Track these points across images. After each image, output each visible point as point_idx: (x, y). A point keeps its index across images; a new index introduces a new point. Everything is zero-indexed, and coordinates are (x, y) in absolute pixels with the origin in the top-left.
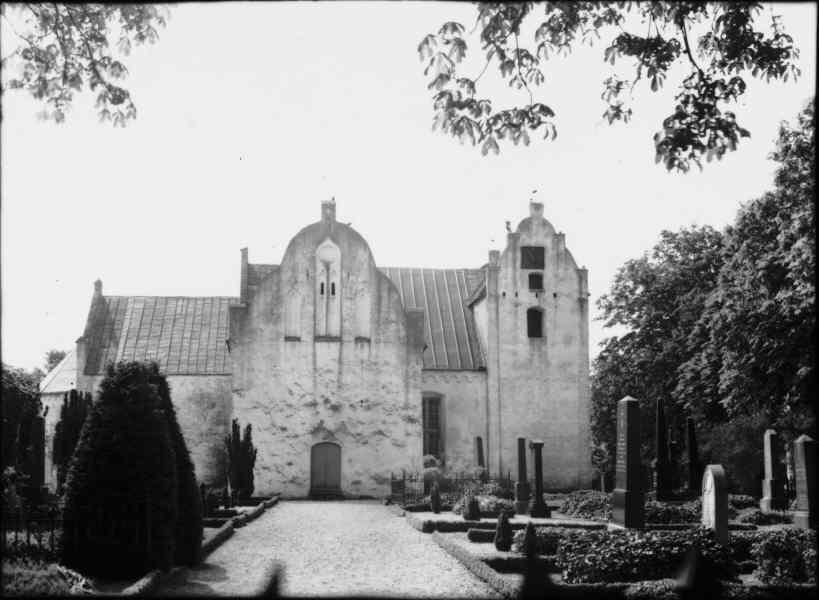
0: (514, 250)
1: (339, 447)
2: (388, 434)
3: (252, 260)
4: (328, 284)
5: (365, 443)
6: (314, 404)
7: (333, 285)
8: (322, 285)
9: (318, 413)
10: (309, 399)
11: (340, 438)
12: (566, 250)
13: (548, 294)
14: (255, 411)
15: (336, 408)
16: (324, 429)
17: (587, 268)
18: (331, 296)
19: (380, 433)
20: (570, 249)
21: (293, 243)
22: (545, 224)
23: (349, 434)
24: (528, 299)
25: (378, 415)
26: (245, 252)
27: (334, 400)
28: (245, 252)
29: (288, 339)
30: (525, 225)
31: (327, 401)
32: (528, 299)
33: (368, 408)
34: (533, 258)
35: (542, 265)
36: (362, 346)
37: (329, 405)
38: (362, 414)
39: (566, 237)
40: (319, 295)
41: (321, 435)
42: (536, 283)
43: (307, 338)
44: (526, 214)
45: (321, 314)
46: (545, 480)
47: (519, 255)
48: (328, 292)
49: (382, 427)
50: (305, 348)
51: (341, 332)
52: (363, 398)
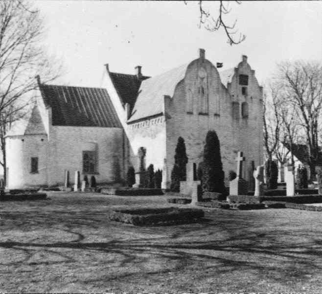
6: (198, 144)
10: (197, 141)
22: (248, 66)
28: (107, 66)
30: (241, 64)
36: (217, 118)
37: (117, 162)
39: (256, 72)
42: (244, 91)
43: (195, 113)
44: (240, 60)
47: (238, 77)
50: (195, 117)
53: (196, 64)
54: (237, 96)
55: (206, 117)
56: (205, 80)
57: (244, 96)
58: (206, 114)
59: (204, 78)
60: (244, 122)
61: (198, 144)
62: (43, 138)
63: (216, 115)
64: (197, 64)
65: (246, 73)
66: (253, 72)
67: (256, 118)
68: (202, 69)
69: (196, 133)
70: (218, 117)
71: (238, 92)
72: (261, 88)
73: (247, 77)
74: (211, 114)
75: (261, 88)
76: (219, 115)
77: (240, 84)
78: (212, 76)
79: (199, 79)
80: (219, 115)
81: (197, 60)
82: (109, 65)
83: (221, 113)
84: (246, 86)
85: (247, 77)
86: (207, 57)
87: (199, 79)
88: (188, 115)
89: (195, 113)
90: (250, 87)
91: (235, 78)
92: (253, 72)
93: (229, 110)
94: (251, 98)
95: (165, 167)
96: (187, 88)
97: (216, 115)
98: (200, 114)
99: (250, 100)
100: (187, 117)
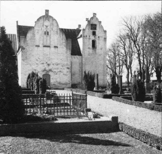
0: (89, 25)
1: (50, 75)
2: (63, 72)
3: (19, 24)
4: (47, 32)
5: (57, 74)
6: (43, 64)
7: (48, 32)
8: (45, 32)
9: (44, 66)
10: (42, 62)
11: (50, 73)
12: (102, 26)
13: (97, 37)
14: (28, 65)
15: (49, 65)
16: (46, 70)
17: (106, 30)
18: (47, 36)
19: (60, 71)
20: (102, 25)
21: (40, 18)
22: (97, 19)
23: (52, 71)
24: (92, 38)
25: (60, 66)
26: (17, 22)
27: (49, 63)
28: (17, 22)
29: (36, 46)
30: (92, 18)
31: (46, 63)
32: (92, 38)
33: (57, 65)
34: (93, 26)
35: (95, 29)
36: (56, 49)
37: (47, 64)
38: (55, 67)
39: (102, 22)
40: (44, 35)
41: (45, 72)
42: (94, 34)
43: (41, 46)
44: (92, 16)
45: (45, 40)
46: (99, 84)
47: (90, 26)
48: (47, 34)
49: (61, 70)
50: (41, 48)
51: (50, 44)
52: (56, 62)
53: (42, 18)
54: (89, 36)
55: (48, 48)
56: (49, 27)
57: (94, 36)
58: (49, 47)
59: (48, 26)
60: (94, 52)
61: (43, 64)
62: (103, 50)
63: (56, 47)
64: (44, 19)
65: (95, 23)
66: (100, 22)
67: (101, 49)
68: (47, 21)
69: (41, 58)
70: (56, 48)
71: (90, 34)
72: (105, 32)
73: (96, 25)
74: (52, 46)
75: (105, 32)
76: (57, 47)
77: (91, 29)
78: (53, 24)
79: (44, 26)
80: (57, 47)
81: (44, 16)
82: (18, 21)
83: (59, 46)
84: (95, 31)
85: (96, 25)
86: (50, 14)
87: (44, 26)
88: (37, 47)
89: (41, 46)
90: (98, 31)
91: (88, 26)
92: (100, 22)
93: (64, 44)
94: (99, 37)
95: (32, 73)
96: (36, 31)
97: (56, 47)
98: (44, 46)
99: (98, 38)
100: (36, 48)
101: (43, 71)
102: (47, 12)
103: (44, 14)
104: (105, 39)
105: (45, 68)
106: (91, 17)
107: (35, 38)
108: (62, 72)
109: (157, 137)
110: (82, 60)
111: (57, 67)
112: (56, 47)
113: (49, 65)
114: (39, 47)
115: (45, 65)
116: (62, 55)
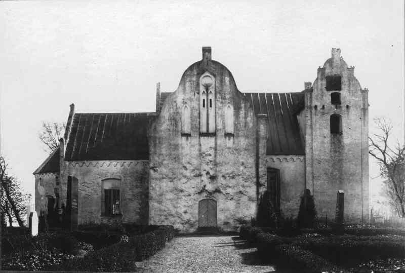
19: (241, 192)
24: (333, 110)
32: (333, 110)
33: (233, 177)
37: (209, 176)
42: (336, 99)
72: (365, 92)
75: (365, 92)
81: (198, 64)
92: (352, 69)
101: (200, 193)
102: (207, 53)
103: (199, 58)
104: (365, 110)
105: (205, 186)
106: (327, 59)
107: (396, 224)
108: (246, 195)
109: (231, 221)
110: (305, 169)
111: (233, 182)
112: (229, 136)
113: (213, 178)
114: (189, 138)
115: (205, 178)
116: (297, 179)
